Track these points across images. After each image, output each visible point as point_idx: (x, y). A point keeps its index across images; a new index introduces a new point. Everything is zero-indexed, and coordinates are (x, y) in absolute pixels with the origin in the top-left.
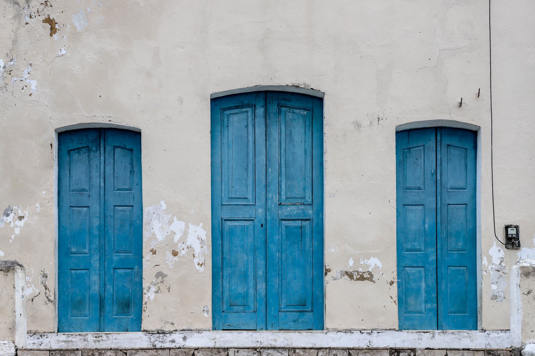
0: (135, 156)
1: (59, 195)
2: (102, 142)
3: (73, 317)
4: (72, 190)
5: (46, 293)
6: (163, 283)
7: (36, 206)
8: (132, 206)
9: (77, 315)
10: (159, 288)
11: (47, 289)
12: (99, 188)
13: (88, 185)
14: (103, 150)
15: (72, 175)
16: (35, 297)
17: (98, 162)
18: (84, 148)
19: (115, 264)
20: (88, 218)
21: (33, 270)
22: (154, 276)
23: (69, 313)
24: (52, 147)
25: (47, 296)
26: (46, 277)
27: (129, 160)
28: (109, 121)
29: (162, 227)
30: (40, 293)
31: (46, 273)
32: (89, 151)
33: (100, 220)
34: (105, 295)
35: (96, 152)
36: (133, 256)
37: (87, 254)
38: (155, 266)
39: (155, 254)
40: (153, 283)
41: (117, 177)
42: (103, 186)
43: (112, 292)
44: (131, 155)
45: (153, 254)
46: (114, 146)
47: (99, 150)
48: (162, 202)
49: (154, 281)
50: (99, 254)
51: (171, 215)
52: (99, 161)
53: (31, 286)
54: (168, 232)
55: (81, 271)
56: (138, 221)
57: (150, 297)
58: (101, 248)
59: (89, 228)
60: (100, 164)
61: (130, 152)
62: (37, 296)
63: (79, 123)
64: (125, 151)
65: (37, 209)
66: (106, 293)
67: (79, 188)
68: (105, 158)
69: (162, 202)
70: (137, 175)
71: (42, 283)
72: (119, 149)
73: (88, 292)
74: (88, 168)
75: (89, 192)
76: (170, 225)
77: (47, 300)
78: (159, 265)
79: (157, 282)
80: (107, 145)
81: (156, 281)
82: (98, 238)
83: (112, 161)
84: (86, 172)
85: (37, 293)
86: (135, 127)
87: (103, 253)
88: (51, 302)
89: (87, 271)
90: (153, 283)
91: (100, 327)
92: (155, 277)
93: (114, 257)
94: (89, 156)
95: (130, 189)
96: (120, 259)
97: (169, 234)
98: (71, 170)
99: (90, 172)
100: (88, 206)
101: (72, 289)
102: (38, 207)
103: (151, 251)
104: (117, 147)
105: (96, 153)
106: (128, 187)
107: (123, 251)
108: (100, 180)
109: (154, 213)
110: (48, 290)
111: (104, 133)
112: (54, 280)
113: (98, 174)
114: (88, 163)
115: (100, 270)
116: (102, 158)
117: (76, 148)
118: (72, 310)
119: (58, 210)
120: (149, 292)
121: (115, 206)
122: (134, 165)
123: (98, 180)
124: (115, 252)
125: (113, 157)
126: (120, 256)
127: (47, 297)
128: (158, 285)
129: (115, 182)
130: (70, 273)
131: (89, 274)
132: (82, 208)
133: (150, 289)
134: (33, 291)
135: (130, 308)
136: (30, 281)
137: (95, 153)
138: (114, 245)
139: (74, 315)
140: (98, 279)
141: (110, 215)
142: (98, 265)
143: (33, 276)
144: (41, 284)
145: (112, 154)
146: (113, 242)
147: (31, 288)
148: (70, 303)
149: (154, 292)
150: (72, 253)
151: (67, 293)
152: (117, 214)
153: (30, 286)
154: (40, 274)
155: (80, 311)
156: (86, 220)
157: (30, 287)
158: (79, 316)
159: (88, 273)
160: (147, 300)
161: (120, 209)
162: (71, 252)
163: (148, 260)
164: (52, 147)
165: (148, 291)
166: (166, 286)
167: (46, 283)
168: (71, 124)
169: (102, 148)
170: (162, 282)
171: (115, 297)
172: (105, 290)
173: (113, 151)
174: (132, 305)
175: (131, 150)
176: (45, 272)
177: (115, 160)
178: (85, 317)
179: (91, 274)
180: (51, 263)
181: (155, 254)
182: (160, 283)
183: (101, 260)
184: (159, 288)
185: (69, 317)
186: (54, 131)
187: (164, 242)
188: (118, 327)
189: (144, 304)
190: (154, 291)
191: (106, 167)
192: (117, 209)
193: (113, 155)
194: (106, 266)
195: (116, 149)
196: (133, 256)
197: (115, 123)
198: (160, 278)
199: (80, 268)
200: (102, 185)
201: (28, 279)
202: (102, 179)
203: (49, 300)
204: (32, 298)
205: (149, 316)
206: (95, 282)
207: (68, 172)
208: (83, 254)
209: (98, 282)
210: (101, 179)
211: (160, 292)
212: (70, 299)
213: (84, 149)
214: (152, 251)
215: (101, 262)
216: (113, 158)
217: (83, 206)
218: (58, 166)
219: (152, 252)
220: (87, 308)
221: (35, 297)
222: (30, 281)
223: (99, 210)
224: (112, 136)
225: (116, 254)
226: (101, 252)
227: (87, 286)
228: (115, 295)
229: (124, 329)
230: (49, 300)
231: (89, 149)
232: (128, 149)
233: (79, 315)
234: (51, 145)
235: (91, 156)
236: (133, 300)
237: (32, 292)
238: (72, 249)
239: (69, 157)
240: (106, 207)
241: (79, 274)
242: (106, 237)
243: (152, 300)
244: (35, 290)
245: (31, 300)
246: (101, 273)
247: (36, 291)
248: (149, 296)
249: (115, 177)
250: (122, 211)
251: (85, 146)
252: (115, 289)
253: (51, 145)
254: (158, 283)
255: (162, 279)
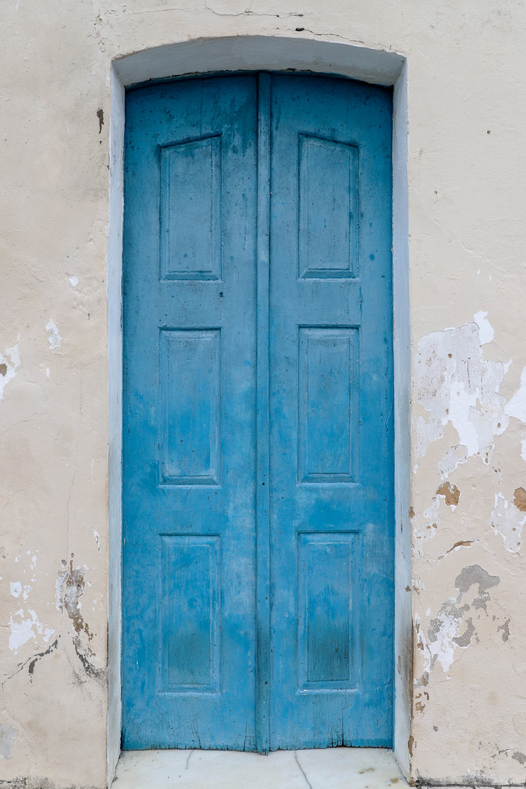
0: (366, 164)
1: (125, 293)
2: (263, 118)
3: (169, 690)
4: (168, 273)
5: (77, 644)
6: (485, 607)
7: (48, 328)
8: (357, 328)
9: (184, 686)
10: (471, 627)
11: (82, 627)
12: (253, 268)
13: (218, 259)
14: (265, 142)
15: (167, 227)
16: (42, 655)
17: (249, 184)
18: (206, 140)
19: (303, 516)
20: (216, 366)
21: (34, 559)
22: (452, 580)
23: (158, 679)
24: (101, 122)
25: (82, 652)
26: (80, 583)
27: (347, 179)
28: (297, 30)
29: (478, 407)
30: (56, 642)
31: (78, 568)
32: (222, 147)
33: (256, 373)
34: (273, 622)
35: (244, 151)
36: (361, 493)
37: (214, 483)
38: (456, 545)
39: (456, 502)
40: (449, 608)
41: (309, 232)
42: (266, 260)
43: (292, 610)
44: (353, 161)
45: (448, 502)
46: (300, 134)
47: (253, 144)
48: (480, 317)
49: (454, 600)
50: (252, 484)
51: (511, 362)
52: (254, 178)
53: (28, 617)
54: (499, 425)
55: (193, 539)
56: (375, 377)
57: (438, 659)
58: (259, 467)
59: (221, 398)
60: (257, 190)
61: (348, 152)
62: (48, 652)
63: (195, 35)
64: (332, 148)
65: (51, 340)
66: (274, 613)
67: (188, 268)
68: (271, 170)
69: (480, 317)
70: (371, 225)
71: (67, 606)
72: (315, 144)
73: (217, 608)
74: (218, 203)
75: (219, 281)
76: (508, 400)
77: (83, 669)
78: (468, 543)
79: (462, 605)
80: (276, 129)
81: (459, 598)
82: (248, 432)
83: (294, 181)
84: (212, 217)
85: (47, 641)
86: (387, 50)
87: (267, 484)
88: (97, 675)
89: (215, 539)
90: (449, 608)
91: (257, 736)
92: (457, 585)
93: (298, 496)
94: (220, 167)
95: (347, 274)
96: (317, 500)
97: (503, 429)
98: (166, 212)
99: (223, 216)
100: (216, 325)
101: (166, 598)
102: (51, 332)
103: (439, 492)
104: (308, 135)
105: (244, 156)
106: (343, 265)
107: (328, 476)
108: (256, 243)
109: (450, 355)
110: (86, 631)
111: (271, 88)
112: (105, 595)
113: (249, 224)
114: (219, 187)
115: (256, 539)
116: (264, 171)
117: (179, 138)
118: (167, 667)
119: (124, 341)
120: (434, 639)
121: (300, 327)
122: (362, 193)
123: (249, 242)
124: (302, 477)
125: (295, 167)
126: (316, 490)
127: (81, 656)
128: (467, 615)
129: (301, 248)
130: (160, 547)
131: (221, 550)
132: (197, 334)
133: (438, 630)
134: (32, 632)
135: (350, 663)
136: (25, 596)
137: (240, 154)
138: (299, 453)
139: (174, 686)
140: (251, 567)
141: (287, 358)
142: (248, 522)
143: (33, 580)
144: (61, 607)
145: (294, 158)
146: (295, 445)
147: (28, 624)
148: (161, 646)
149: (455, 639)
150: (165, 481)
151: (149, 614)
152: (307, 352)
153: (23, 616)
154: (60, 573)
155: (192, 673)
156: (210, 371)
157: (26, 618)
158: (187, 688)
159: (217, 548)
160: (427, 670)
161: (317, 338)
162: (163, 477)
163: (431, 525)
164: (101, 122)
165: (432, 636)
166: (494, 618)
167: (78, 607)
168: (167, 42)
169: (263, 138)
170: (481, 604)
171: (301, 628)
172: (271, 605)
173: (296, 149)
174: (356, 654)
175: (353, 146)
176: (76, 567)
177: (302, 177)
178: (208, 694)
179: (228, 550)
180: (96, 533)
181: (456, 502)
182: (472, 609)
183: (260, 507)
184: (471, 627)
185: (157, 691)
186: (108, 64)
187: (486, 460)
188: (314, 729)
189: (419, 685)
190: (453, 636)
191: (274, 201)
192: (308, 335)
193: (295, 162)
194: (275, 525)
195: (305, 143)
196: (361, 493)
197: (318, 38)
198: (475, 587)
199: (190, 531)
200: (263, 257)
201: (16, 591)
202: (263, 240)
203: (89, 669)
204: (31, 660)
205: (435, 729)
206: (238, 577)
207: (155, 217)
208: (199, 484)
209: (248, 578)
210: (260, 239)
211: (472, 639)
212: (159, 631)
213: (204, 143)
214: (443, 490)
215: (259, 514)
216: (296, 171)
217: (199, 326)
218: (125, 196)
219: (444, 496)
220: (216, 663)
221: (42, 655)
222: (25, 596)
223: (253, 339)
224: (294, 99)
225: (303, 484)
226: (260, 483)
227: (214, 592)
228: (301, 621)
229: (331, 733)
230: (87, 669)
231: (221, 143)
232: (342, 143)
233: (187, 686)
234: (100, 114)
235: (229, 166)
236: (357, 634)
237: (32, 638)
238: (167, 466)
239: (160, 168)
240: (273, 329)
241: (189, 548)
242: (275, 429)
243: (446, 669)
244: (40, 631)
245: (27, 668)
246: (259, 550)
247: (44, 635)
248: (436, 656)
249: (301, 231)
250: (323, 342)
251: (210, 131)
252: (304, 601)
253: (100, 114)
254: (467, 608)
255: (481, 592)
